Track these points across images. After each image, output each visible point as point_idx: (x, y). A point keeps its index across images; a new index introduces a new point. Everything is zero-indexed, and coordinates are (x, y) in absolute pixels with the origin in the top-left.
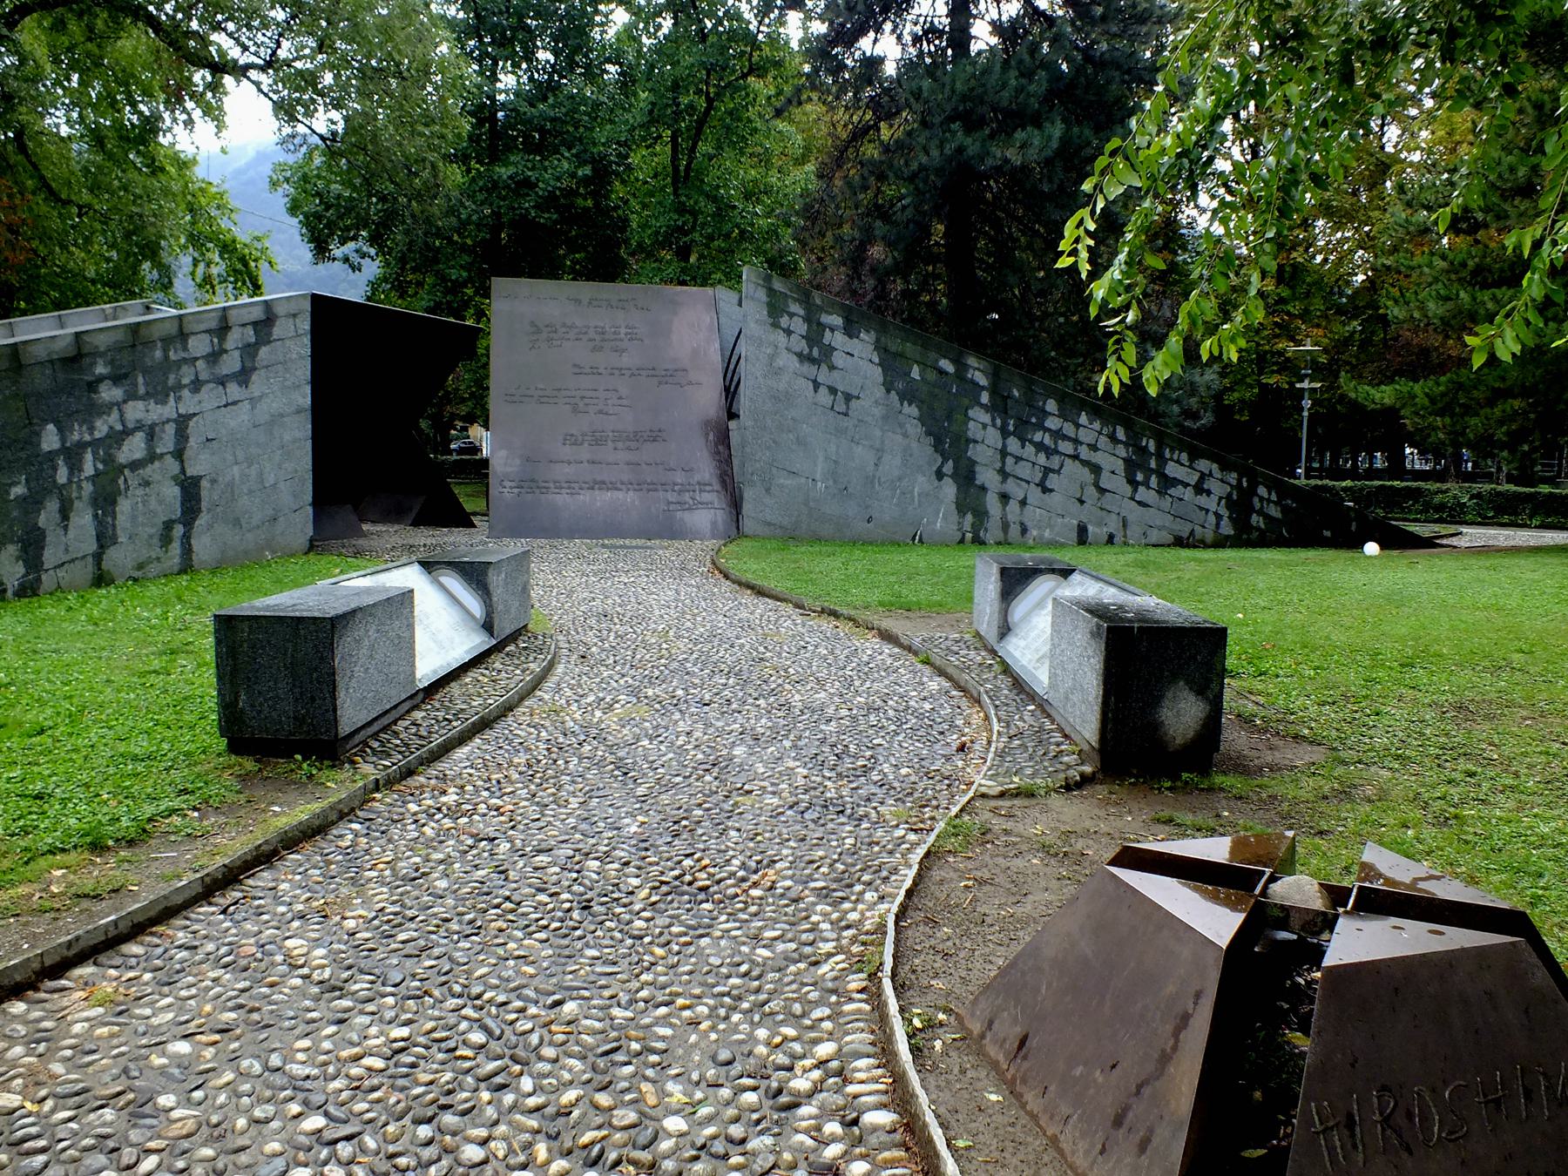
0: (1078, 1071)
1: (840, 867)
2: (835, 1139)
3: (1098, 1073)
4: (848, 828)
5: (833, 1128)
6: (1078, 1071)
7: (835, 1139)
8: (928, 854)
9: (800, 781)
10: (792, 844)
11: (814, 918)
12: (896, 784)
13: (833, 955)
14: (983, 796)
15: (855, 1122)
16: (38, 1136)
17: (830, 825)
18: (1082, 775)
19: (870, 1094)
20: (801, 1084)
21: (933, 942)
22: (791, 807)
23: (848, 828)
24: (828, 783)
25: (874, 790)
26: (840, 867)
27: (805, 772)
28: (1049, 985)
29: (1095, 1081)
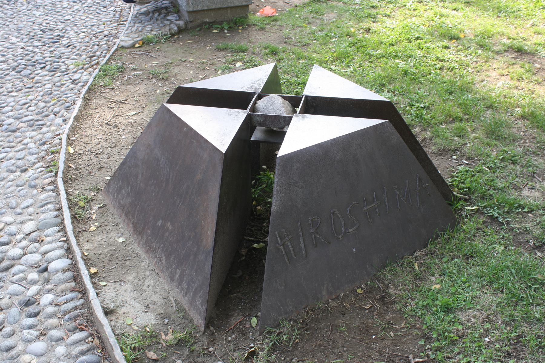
0: (160, 223)
1: (42, 105)
2: (33, 282)
3: (169, 224)
4: (48, 78)
5: (33, 275)
6: (160, 223)
7: (33, 282)
8: (89, 89)
9: (20, 51)
10: (14, 94)
11: (25, 141)
12: (77, 44)
13: (36, 163)
14: (123, 47)
15: (46, 269)
16: (4, 103)
17: (37, 78)
18: (179, 27)
19: (54, 249)
20: (15, 251)
21: (89, 147)
22: (14, 69)
23: (48, 78)
24: (37, 50)
25: (63, 50)
26: (42, 105)
27: (22, 44)
28: (142, 174)
29: (168, 228)
